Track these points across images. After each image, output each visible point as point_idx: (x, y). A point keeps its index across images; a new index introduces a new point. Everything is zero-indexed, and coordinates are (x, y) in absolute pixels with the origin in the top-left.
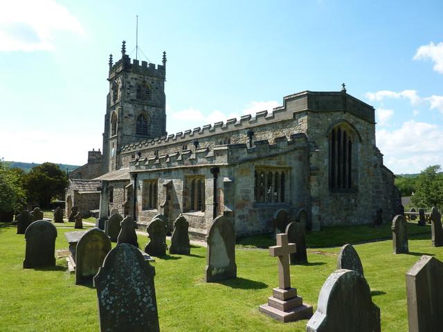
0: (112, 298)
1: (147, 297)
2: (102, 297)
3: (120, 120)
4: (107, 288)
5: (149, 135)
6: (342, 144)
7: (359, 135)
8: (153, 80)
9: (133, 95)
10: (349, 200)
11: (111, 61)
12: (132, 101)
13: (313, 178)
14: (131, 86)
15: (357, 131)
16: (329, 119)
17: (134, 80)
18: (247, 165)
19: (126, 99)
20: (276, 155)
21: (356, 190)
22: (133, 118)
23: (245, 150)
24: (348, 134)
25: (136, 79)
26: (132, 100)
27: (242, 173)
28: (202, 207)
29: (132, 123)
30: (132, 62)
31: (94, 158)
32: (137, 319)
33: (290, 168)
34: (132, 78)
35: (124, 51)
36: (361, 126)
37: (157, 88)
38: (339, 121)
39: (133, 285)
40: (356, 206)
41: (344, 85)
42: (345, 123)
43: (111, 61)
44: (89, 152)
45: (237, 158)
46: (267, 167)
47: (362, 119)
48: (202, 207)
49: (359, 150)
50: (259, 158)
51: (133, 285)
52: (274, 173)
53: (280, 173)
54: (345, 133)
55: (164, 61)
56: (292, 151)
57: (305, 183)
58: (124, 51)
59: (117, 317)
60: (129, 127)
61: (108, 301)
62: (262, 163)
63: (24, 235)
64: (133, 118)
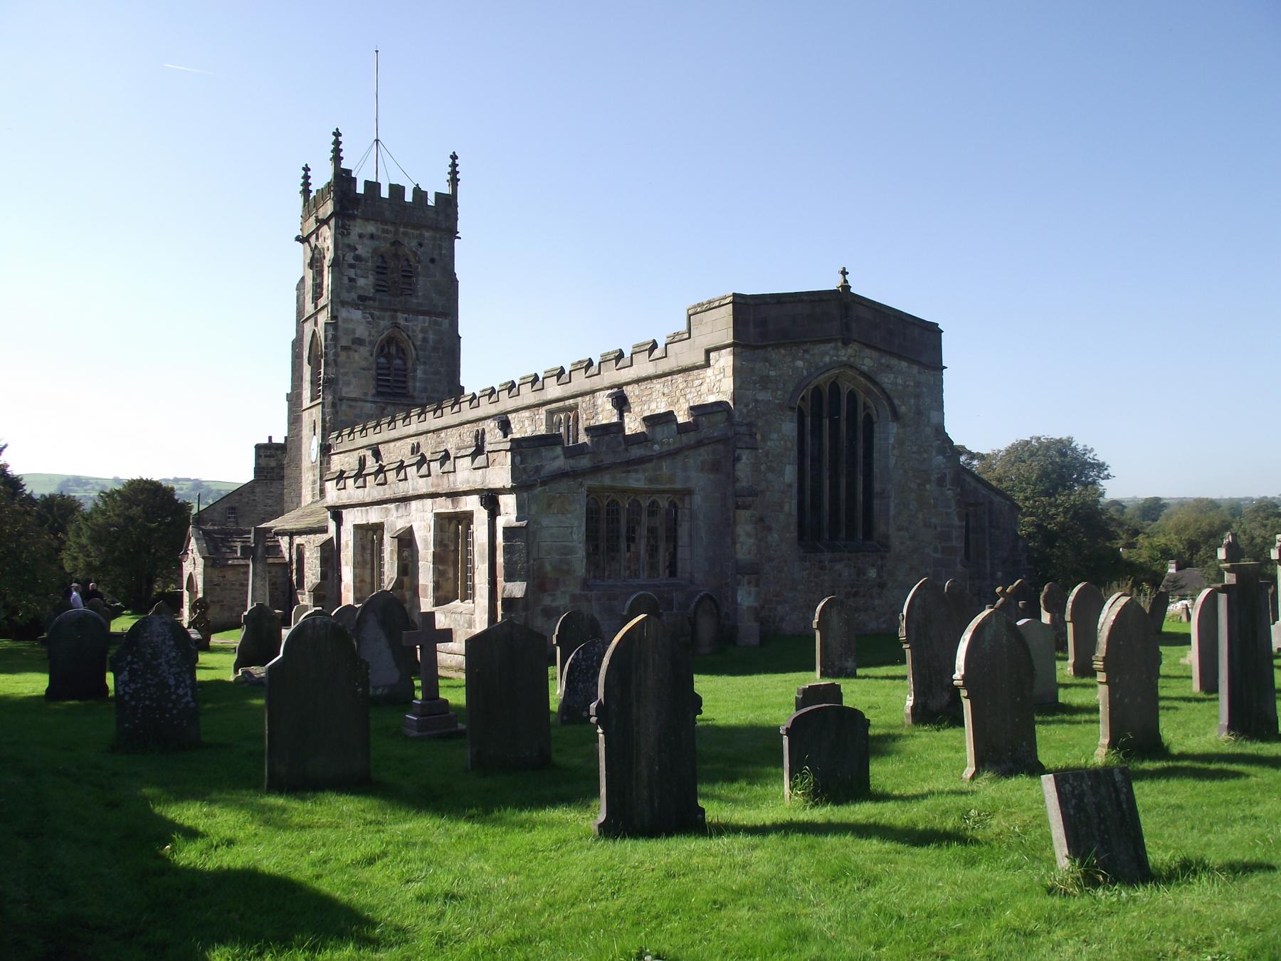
0: (133, 686)
1: (183, 689)
2: (120, 683)
4: (126, 673)
5: (413, 397)
6: (843, 426)
7: (889, 399)
8: (421, 235)
9: (365, 283)
10: (860, 572)
11: (306, 184)
13: (743, 515)
14: (358, 258)
15: (883, 391)
16: (800, 363)
17: (367, 242)
18: (562, 486)
19: (345, 296)
20: (641, 461)
21: (885, 546)
22: (364, 351)
23: (559, 450)
24: (861, 397)
25: (372, 237)
26: (362, 298)
27: (549, 506)
28: (468, 594)
29: (364, 364)
30: (360, 189)
32: (167, 715)
33: (689, 492)
34: (361, 236)
35: (337, 157)
36: (897, 376)
37: (432, 261)
38: (829, 367)
39: (164, 671)
40: (882, 586)
41: (844, 273)
42: (850, 372)
43: (306, 184)
44: (259, 448)
45: (538, 469)
46: (624, 491)
47: (901, 357)
48: (468, 594)
49: (892, 441)
50: (596, 470)
51: (164, 671)
52: (645, 503)
53: (664, 503)
54: (852, 396)
55: (454, 181)
56: (690, 447)
57: (724, 531)
58: (337, 157)
59: (140, 711)
61: (127, 689)
62: (607, 480)
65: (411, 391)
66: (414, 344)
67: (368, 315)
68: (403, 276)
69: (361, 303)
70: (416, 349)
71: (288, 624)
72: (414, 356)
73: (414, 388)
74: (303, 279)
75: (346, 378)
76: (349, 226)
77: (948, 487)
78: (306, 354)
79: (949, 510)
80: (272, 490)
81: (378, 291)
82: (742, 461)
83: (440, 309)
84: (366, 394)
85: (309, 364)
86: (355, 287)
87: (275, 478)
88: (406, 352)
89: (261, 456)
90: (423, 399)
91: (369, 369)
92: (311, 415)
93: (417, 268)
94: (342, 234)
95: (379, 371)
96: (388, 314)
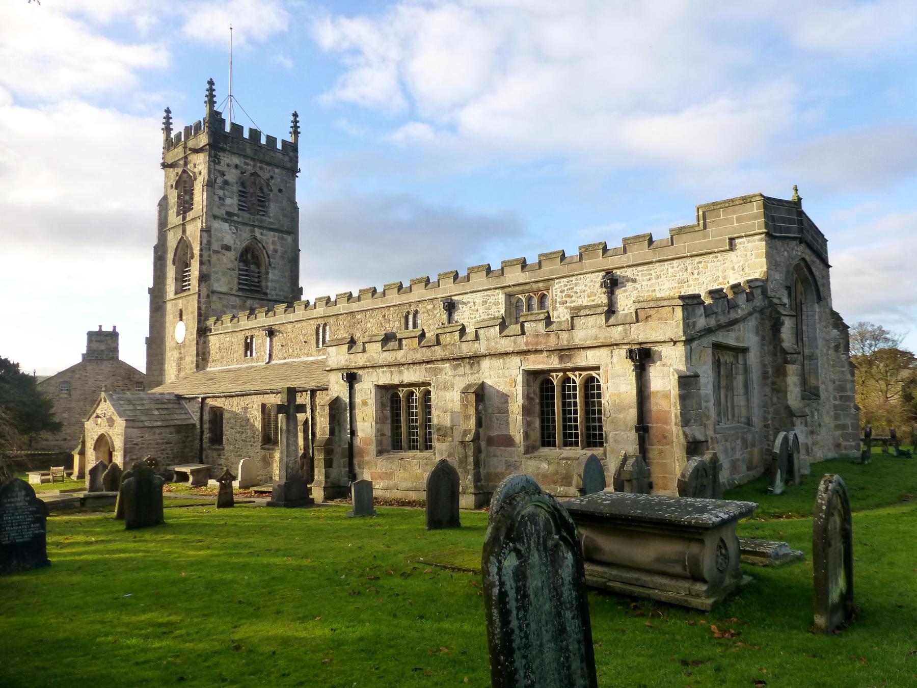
3: (205, 258)
5: (266, 294)
9: (232, 202)
12: (228, 217)
14: (226, 183)
19: (217, 211)
29: (230, 266)
30: (228, 129)
31: (103, 347)
34: (228, 165)
35: (211, 100)
37: (280, 191)
44: (91, 335)
58: (211, 100)
60: (224, 274)
63: (124, 522)
64: (231, 255)
65: (264, 288)
66: (267, 252)
67: (233, 228)
68: (259, 200)
69: (229, 218)
70: (269, 257)
71: (235, 478)
72: (267, 262)
73: (267, 287)
74: (165, 198)
75: (217, 275)
76: (220, 156)
77: (842, 352)
78: (170, 256)
79: (843, 369)
80: (102, 368)
81: (240, 209)
82: (785, 326)
83: (286, 228)
84: (231, 289)
85: (174, 263)
86: (223, 205)
87: (105, 358)
88: (259, 259)
89: (92, 341)
90: (272, 296)
91: (234, 270)
92: (176, 305)
93: (269, 195)
94: (214, 162)
95: (240, 272)
96: (249, 228)
